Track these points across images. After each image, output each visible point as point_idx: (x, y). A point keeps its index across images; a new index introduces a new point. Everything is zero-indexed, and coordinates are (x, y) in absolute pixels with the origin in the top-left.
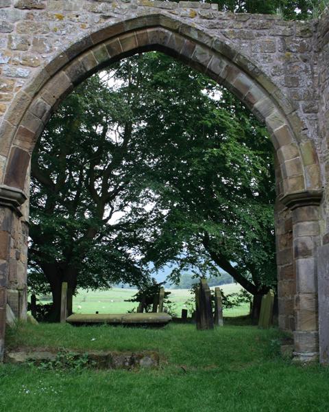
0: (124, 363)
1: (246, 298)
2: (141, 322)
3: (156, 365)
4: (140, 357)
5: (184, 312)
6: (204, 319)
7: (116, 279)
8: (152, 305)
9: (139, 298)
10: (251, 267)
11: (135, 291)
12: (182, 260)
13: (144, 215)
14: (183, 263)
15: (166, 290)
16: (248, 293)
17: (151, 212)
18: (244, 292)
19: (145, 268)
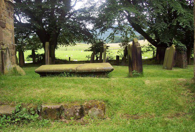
0: (74, 113)
1: (151, 49)
2: (91, 71)
3: (103, 114)
4: (89, 108)
5: (118, 57)
6: (135, 66)
7: (79, 40)
8: (99, 53)
9: (92, 49)
10: (156, 32)
11: (90, 45)
12: (115, 28)
13: (94, 4)
14: (116, 29)
15: (108, 45)
16: (153, 46)
17: (98, 2)
18: (150, 46)
19: (95, 33)
